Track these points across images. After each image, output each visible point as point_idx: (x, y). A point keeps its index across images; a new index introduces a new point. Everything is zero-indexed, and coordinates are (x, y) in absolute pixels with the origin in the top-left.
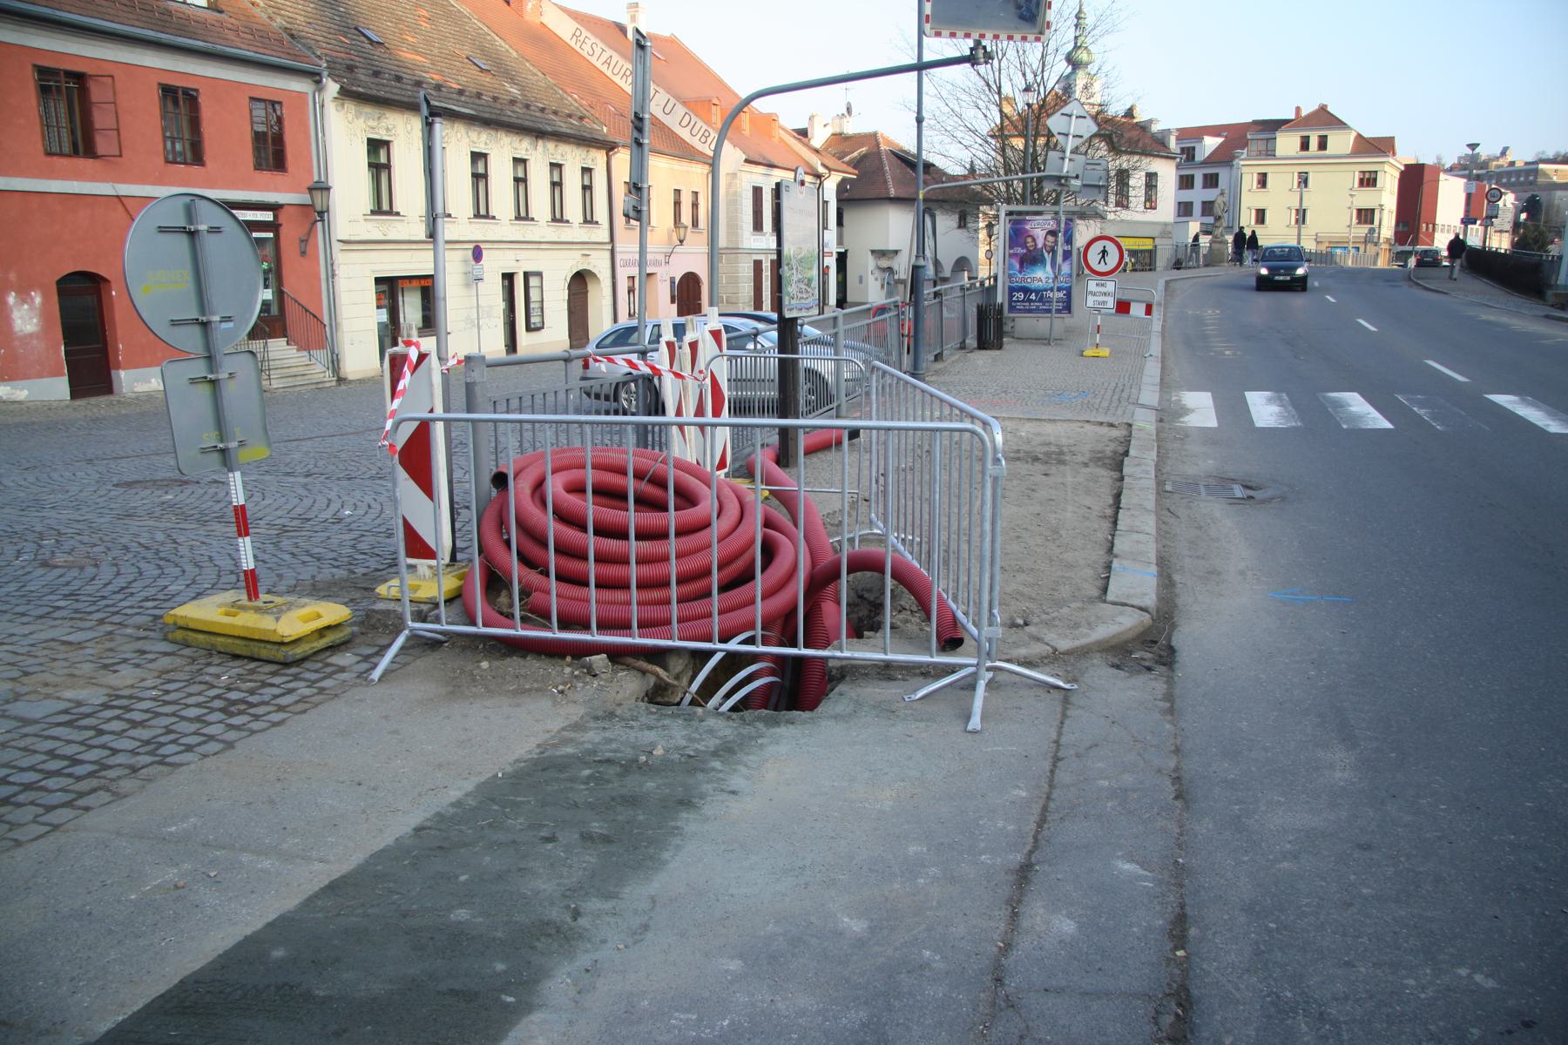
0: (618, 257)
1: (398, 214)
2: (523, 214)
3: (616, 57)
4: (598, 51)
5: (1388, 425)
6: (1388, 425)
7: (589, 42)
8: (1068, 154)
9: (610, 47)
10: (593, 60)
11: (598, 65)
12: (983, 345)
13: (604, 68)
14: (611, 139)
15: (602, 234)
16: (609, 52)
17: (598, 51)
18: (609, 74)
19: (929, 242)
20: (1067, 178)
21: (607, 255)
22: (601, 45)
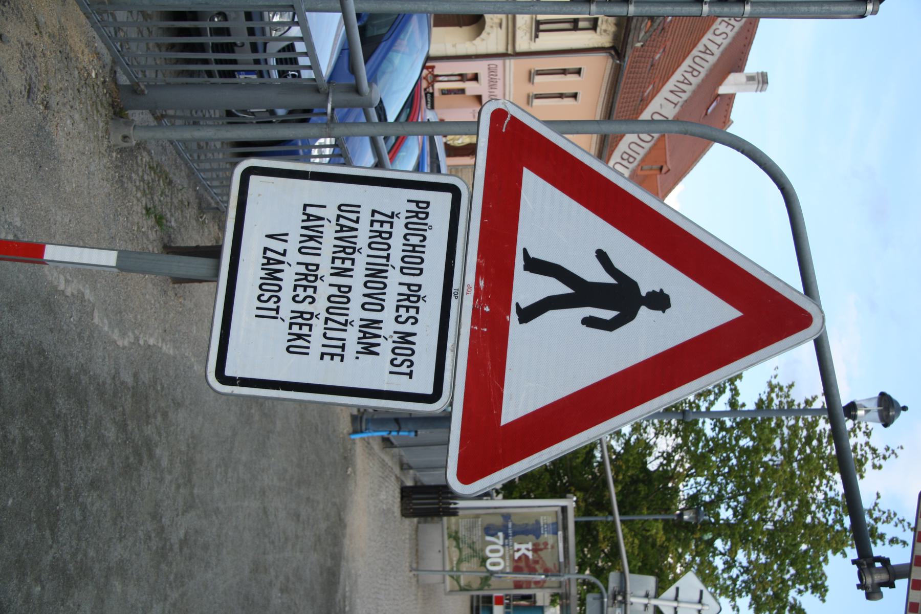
0: (498, 62)
1: (537, 36)
2: (542, 27)
3: (712, 60)
4: (719, 40)
5: (615, 282)
6: (615, 282)
7: (728, 30)
8: (654, 602)
9: (723, 54)
10: (709, 35)
11: (704, 40)
12: (406, 493)
13: (700, 47)
14: (629, 52)
15: (523, 44)
16: (717, 52)
17: (719, 40)
18: (695, 52)
19: (446, 79)
20: (624, 602)
21: (501, 49)
22: (726, 43)
